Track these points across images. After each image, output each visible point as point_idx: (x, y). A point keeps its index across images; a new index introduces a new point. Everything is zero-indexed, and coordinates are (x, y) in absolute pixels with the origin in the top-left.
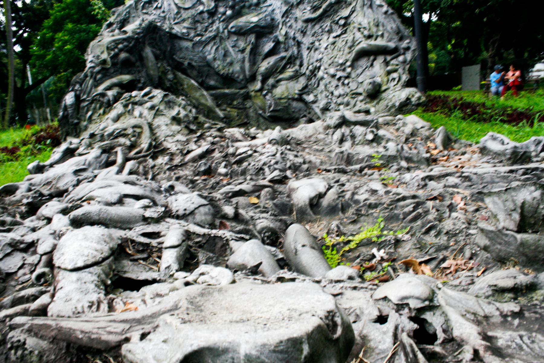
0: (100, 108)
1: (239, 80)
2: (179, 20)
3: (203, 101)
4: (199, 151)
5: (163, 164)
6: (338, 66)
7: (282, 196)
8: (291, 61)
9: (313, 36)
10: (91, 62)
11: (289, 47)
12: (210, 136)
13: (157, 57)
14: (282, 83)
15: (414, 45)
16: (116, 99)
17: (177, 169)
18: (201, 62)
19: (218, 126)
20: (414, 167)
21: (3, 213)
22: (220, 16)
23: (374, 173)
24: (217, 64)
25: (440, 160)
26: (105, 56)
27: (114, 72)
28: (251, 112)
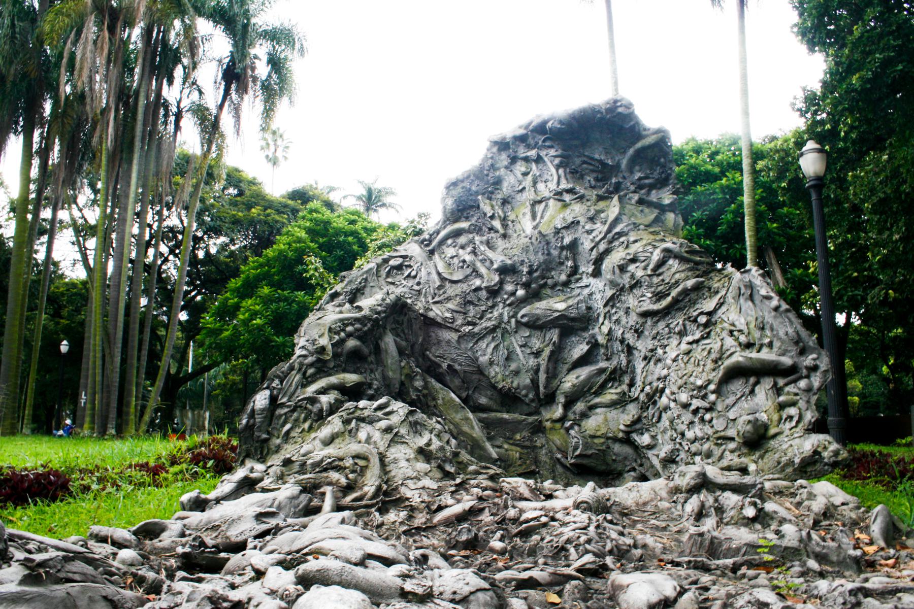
0: (305, 421)
1: (527, 400)
2: (442, 298)
3: (466, 429)
4: (457, 509)
5: (397, 523)
6: (693, 390)
7: (599, 596)
8: (615, 376)
9: (654, 338)
10: (303, 347)
11: (613, 353)
12: (477, 486)
13: (401, 352)
14: (598, 410)
15: (824, 363)
16: (333, 409)
17: (419, 533)
18: (469, 365)
19: (491, 472)
20: (831, 572)
21: (143, 564)
22: (505, 296)
23: (759, 574)
24: (495, 372)
25: (881, 565)
26: (324, 341)
27: (334, 367)
28: (543, 456)
